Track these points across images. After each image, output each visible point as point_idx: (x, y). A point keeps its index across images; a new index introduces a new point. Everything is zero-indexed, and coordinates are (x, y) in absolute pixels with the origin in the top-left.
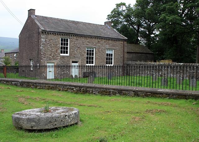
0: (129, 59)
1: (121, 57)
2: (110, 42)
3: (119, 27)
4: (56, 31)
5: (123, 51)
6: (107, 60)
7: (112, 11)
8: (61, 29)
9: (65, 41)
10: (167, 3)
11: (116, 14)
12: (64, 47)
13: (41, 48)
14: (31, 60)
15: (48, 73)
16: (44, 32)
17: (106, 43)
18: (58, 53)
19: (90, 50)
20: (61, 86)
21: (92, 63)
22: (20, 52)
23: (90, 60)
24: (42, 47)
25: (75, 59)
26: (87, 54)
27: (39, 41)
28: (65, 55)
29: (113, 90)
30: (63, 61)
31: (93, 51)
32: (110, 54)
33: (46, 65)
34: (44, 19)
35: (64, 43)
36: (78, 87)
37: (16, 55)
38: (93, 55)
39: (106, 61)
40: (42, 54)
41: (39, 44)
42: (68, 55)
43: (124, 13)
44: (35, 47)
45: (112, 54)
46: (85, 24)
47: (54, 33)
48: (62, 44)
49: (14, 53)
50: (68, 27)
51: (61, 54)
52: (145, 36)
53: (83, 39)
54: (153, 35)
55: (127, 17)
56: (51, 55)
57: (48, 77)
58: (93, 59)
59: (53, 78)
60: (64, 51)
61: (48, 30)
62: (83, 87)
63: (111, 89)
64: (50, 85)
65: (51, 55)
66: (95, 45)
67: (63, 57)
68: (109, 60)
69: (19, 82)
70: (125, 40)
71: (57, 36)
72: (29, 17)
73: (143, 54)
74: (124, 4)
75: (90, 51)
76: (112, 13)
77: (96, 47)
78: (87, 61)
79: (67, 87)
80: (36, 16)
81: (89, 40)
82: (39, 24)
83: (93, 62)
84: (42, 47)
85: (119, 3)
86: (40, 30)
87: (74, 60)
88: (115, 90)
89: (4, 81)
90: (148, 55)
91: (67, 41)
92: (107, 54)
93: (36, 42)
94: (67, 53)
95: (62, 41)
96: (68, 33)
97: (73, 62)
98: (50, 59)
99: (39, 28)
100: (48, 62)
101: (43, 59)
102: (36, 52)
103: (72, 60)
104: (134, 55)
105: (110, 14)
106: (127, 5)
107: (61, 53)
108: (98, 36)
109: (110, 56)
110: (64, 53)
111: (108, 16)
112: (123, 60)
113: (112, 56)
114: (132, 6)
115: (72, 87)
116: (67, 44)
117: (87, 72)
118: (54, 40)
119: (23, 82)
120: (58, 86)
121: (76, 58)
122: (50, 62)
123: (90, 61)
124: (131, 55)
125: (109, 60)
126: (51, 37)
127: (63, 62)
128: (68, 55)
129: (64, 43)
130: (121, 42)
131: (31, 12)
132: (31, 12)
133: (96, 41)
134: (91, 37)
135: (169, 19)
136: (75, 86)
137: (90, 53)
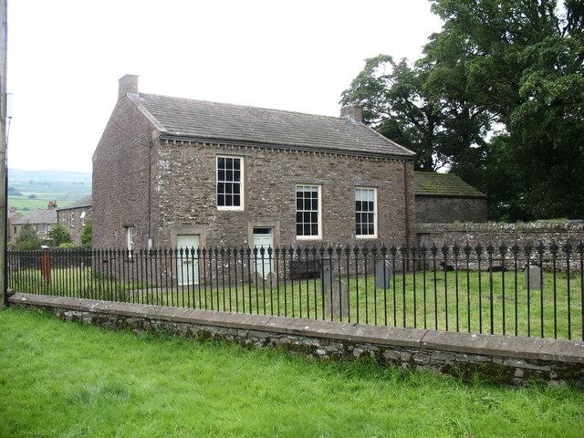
0: (424, 217)
1: (400, 212)
2: (366, 164)
3: (377, 122)
4: (205, 136)
5: (403, 191)
6: (358, 220)
7: (354, 80)
8: (221, 132)
9: (229, 166)
10: (541, 40)
11: (366, 88)
12: (228, 186)
13: (159, 188)
14: (127, 227)
15: (180, 268)
16: (166, 139)
17: (355, 169)
18: (212, 204)
19: (307, 191)
20: (259, 334)
21: (315, 233)
22: (94, 206)
23: (306, 223)
24: (162, 185)
25: (526, 232)
26: (299, 206)
27: (153, 167)
28: (233, 208)
29: (528, 361)
30: (226, 229)
31: (315, 194)
32: (365, 203)
33: (173, 249)
34: (162, 106)
35: (229, 173)
36: (337, 341)
37: (86, 216)
38: (315, 207)
39: (354, 224)
40: (161, 209)
41: (152, 176)
42: (241, 208)
43: (389, 85)
44: (138, 187)
45: (372, 204)
46: (285, 116)
47: (198, 141)
48: (221, 176)
49: (80, 209)
50: (237, 124)
51: (220, 208)
52: (452, 147)
53: (284, 158)
54: (475, 146)
55: (400, 94)
56: (188, 211)
57: (180, 279)
58: (315, 219)
59: (196, 283)
60: (229, 198)
61: (178, 133)
62: (364, 343)
63: (513, 358)
64: (209, 329)
65: (188, 211)
66: (322, 176)
67: (227, 215)
68: (364, 221)
69: (86, 310)
70: (406, 158)
71: (205, 150)
72: (122, 97)
73: (457, 201)
74: (389, 59)
75: (307, 194)
76: (353, 85)
77: (326, 182)
78: (299, 227)
79: (284, 340)
80: (141, 95)
81: (303, 160)
82: (151, 118)
83: (315, 227)
84: (162, 185)
85: (373, 56)
86: (155, 135)
87: (260, 225)
88: (541, 362)
89: (39, 306)
90: (470, 202)
91: (237, 166)
92: (358, 203)
93: (144, 170)
94: (237, 203)
95: (221, 165)
96: (235, 149)
97: (258, 231)
98: (187, 224)
99: (150, 129)
100: (180, 233)
101: (165, 224)
102: (144, 202)
103: (255, 224)
104: (431, 204)
105: (349, 88)
106: (397, 61)
107: (221, 203)
108: (331, 147)
109: (365, 209)
110: (229, 204)
111: (344, 93)
112: (407, 221)
113: (372, 209)
114: (411, 66)
115: (308, 342)
116: (237, 174)
117: (299, 262)
118: (197, 164)
119: (103, 312)
120: (243, 334)
121: (266, 219)
122: (185, 233)
123: (307, 227)
124: (424, 204)
125: (364, 221)
126: (188, 153)
127: (226, 230)
128: (241, 208)
129: (229, 173)
130: (396, 165)
131: (128, 84)
132: (128, 84)
133: (325, 161)
134: (308, 151)
135: (551, 87)
136: (325, 340)
137: (307, 201)
